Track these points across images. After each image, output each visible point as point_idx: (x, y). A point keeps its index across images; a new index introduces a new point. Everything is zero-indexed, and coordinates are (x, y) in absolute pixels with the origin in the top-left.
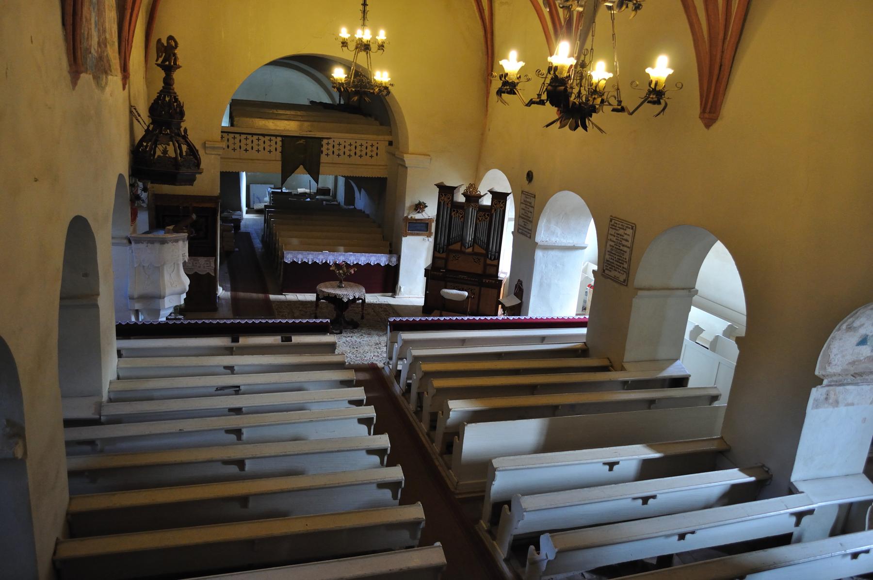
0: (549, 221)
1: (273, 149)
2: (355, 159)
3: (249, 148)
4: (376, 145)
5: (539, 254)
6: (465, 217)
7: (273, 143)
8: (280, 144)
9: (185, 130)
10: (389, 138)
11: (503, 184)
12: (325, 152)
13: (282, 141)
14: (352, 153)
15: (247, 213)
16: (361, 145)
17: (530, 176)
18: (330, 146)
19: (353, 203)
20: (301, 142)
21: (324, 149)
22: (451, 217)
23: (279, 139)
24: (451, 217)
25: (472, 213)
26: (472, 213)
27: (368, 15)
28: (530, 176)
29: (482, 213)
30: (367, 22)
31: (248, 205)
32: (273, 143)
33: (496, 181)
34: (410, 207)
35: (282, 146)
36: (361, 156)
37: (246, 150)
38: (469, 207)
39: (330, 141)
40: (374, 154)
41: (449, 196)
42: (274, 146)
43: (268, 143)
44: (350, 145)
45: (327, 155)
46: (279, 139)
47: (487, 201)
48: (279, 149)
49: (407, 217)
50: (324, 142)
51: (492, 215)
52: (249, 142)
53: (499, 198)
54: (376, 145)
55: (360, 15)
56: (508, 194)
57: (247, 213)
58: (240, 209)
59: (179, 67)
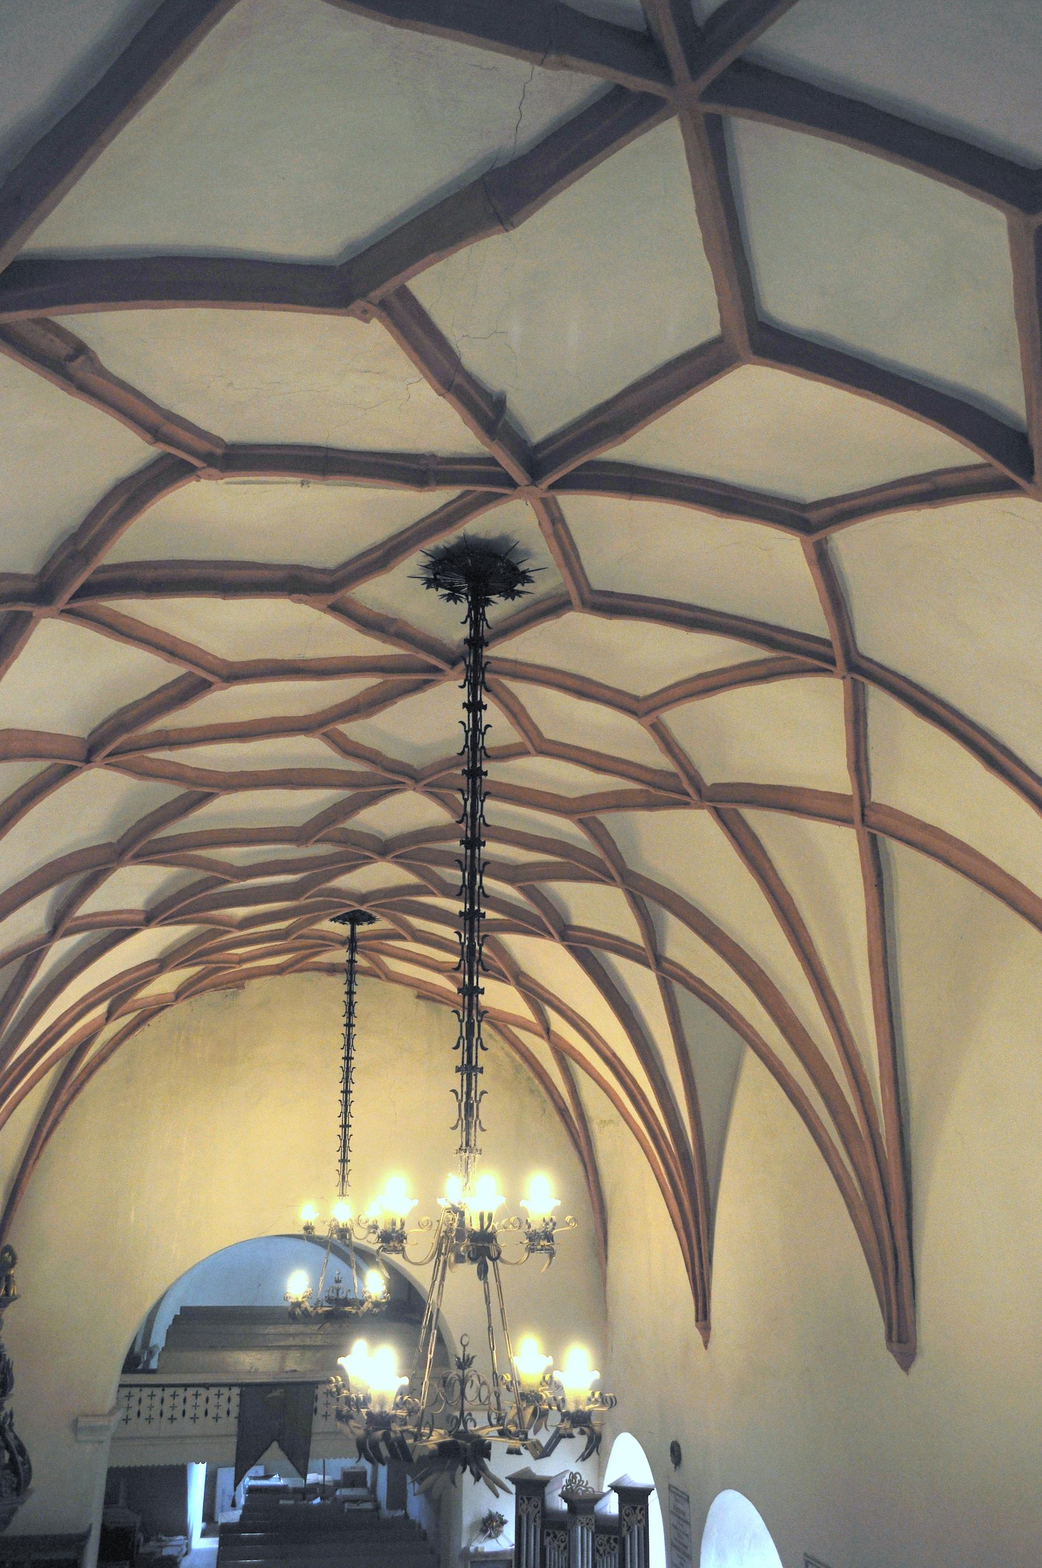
0: (722, 1555)
3: (178, 1414)
6: (569, 1548)
7: (223, 1400)
8: (236, 1400)
11: (641, 1475)
12: (321, 1410)
13: (241, 1395)
15: (204, 1534)
17: (676, 1453)
19: (403, 1505)
20: (276, 1393)
22: (543, 1550)
23: (236, 1391)
24: (543, 1550)
25: (582, 1536)
26: (582, 1536)
27: (350, 1178)
28: (676, 1453)
29: (603, 1538)
30: (348, 1190)
31: (209, 1516)
32: (223, 1400)
33: (628, 1461)
34: (473, 1527)
35: (241, 1405)
38: (575, 1523)
41: (536, 1500)
46: (236, 1391)
47: (611, 1506)
48: (235, 1411)
49: (467, 1549)
51: (624, 1539)
53: (633, 1498)
55: (337, 1178)
56: (645, 1492)
57: (204, 1534)
58: (184, 1530)
59: (458, 1070)
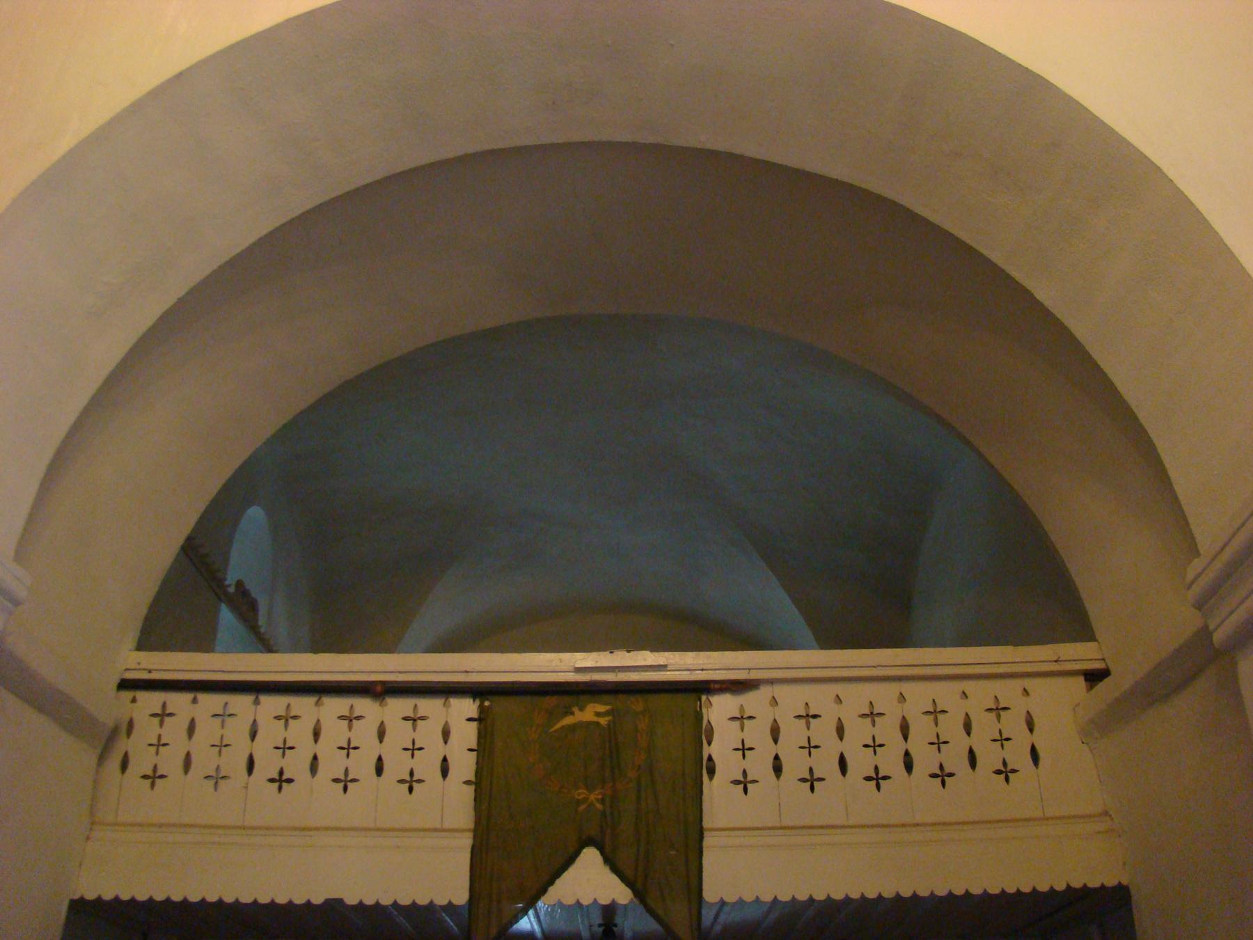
1: (427, 766)
2: (913, 796)
3: (296, 765)
4: (1019, 706)
5: (472, 826)
9: (239, 584)
10: (1081, 654)
13: (482, 719)
14: (890, 762)
16: (998, 710)
18: (757, 734)
20: (590, 712)
21: (720, 749)
36: (942, 775)
37: (281, 780)
39: (752, 701)
40: (1018, 756)
42: (434, 750)
43: (400, 734)
44: (872, 715)
45: (744, 783)
48: (464, 765)
50: (719, 709)
52: (299, 733)
54: (1019, 706)
